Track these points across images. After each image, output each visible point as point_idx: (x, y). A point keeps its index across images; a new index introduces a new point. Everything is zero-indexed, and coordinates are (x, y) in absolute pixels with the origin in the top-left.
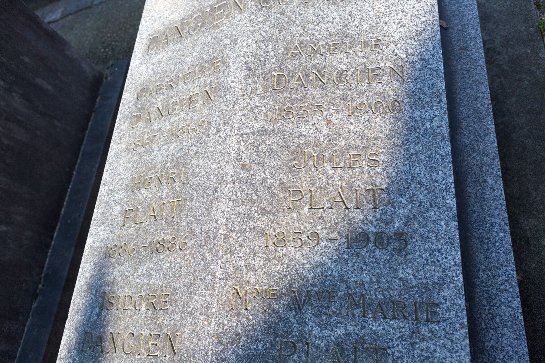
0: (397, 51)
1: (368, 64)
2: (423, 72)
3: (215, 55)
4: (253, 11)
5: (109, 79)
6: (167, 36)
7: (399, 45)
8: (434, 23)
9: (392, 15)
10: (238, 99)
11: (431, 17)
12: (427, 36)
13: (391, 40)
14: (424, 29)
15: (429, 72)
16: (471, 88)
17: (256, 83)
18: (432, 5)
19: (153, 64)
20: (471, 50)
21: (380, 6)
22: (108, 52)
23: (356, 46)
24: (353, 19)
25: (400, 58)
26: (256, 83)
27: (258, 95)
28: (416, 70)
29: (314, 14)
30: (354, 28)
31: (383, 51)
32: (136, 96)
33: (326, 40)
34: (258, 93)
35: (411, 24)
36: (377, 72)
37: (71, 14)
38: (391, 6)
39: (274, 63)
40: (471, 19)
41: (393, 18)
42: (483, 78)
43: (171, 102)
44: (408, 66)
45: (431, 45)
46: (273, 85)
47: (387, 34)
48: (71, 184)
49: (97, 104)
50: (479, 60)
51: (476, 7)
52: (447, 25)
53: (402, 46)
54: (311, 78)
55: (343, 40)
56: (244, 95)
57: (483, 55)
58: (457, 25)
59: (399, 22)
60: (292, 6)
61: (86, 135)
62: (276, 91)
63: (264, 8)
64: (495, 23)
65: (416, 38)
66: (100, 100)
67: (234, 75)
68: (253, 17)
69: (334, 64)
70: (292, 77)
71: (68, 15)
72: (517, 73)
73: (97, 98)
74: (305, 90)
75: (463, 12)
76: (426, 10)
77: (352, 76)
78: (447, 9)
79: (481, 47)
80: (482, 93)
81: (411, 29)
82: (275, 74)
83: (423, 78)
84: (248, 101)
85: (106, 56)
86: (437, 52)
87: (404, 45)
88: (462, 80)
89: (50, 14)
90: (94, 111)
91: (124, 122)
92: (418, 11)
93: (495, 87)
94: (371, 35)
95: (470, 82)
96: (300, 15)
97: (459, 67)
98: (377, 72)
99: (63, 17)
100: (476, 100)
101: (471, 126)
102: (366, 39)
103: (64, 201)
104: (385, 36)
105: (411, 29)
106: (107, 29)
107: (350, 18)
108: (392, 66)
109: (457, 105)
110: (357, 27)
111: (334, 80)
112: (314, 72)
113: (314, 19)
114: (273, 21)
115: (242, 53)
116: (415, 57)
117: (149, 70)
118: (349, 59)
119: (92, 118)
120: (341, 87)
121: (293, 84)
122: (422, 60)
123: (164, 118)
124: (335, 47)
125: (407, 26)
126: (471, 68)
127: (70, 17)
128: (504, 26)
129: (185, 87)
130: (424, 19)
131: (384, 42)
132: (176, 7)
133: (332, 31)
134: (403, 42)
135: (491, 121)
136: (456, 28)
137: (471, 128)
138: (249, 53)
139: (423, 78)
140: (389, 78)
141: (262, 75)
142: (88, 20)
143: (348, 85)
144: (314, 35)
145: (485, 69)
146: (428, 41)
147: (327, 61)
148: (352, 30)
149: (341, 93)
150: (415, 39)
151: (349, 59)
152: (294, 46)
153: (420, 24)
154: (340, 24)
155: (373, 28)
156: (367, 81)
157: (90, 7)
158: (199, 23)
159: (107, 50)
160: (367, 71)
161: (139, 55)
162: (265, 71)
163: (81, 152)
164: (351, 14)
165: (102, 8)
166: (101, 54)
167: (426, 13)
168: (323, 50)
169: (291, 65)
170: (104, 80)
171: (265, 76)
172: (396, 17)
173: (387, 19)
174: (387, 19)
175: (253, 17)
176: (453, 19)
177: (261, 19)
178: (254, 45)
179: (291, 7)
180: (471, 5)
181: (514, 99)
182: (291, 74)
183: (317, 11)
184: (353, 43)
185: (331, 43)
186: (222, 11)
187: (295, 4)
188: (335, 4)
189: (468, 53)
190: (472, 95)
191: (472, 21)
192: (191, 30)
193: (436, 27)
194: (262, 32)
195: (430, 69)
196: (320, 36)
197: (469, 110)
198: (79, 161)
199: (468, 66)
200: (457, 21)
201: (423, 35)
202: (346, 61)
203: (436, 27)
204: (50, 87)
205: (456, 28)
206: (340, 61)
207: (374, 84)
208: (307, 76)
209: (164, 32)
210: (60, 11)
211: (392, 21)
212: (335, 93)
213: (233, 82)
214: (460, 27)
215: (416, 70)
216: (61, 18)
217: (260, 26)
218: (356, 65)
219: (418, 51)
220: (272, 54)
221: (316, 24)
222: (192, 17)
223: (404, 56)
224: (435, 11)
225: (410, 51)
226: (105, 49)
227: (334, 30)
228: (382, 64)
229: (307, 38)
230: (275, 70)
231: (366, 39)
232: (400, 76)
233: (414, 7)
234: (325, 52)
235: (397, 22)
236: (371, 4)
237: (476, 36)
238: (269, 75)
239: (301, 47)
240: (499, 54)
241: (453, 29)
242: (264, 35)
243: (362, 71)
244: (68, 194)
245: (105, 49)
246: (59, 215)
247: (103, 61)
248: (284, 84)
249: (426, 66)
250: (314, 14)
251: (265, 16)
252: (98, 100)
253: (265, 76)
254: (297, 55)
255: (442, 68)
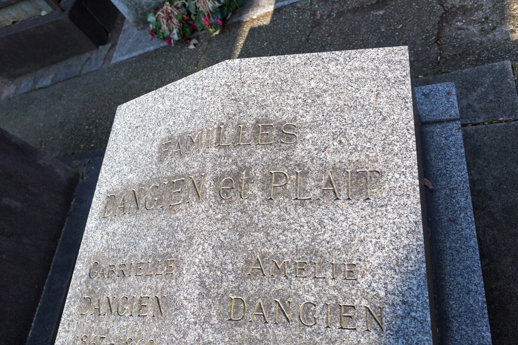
0: (374, 285)
1: (340, 300)
2: (405, 321)
3: (169, 250)
4: (211, 204)
5: (85, 178)
6: (124, 200)
7: (377, 277)
8: (419, 250)
9: (369, 231)
10: (188, 327)
11: (415, 240)
12: (410, 268)
13: (368, 266)
14: (407, 257)
15: (413, 323)
16: (463, 277)
17: (210, 307)
18: (416, 223)
19: (108, 234)
20: (461, 224)
21: (355, 215)
22: (92, 129)
23: (326, 271)
24: (323, 230)
25: (377, 295)
26: (210, 307)
27: (212, 325)
28: (397, 317)
29: (279, 217)
30: (324, 243)
31: (358, 283)
32: (88, 272)
33: (292, 257)
34: (212, 322)
35: (391, 247)
36: (351, 313)
37: (60, 82)
38: (367, 217)
39: (232, 281)
40: (460, 182)
41: (370, 235)
42: (476, 264)
43: (121, 296)
44: (387, 310)
45: (415, 282)
46: (230, 314)
47: (363, 258)
48: (41, 301)
49: (72, 207)
50: (471, 239)
51: (466, 167)
52: (433, 186)
53: (380, 278)
54: (273, 310)
55: (311, 258)
56: (195, 323)
57: (475, 232)
58: (444, 188)
59: (377, 242)
60: (255, 203)
61: (59, 244)
62: (233, 322)
63: (224, 202)
64: (485, 159)
65: (397, 268)
66: (75, 202)
67: (187, 290)
68: (211, 211)
69: (301, 293)
70: (252, 304)
71: (57, 82)
72: (512, 227)
73: (72, 201)
74: (266, 327)
75: (450, 171)
76: (408, 229)
77: (321, 314)
78: (433, 165)
79: (472, 222)
80: (475, 285)
81: (391, 255)
82: (233, 297)
83: (406, 331)
84: (200, 332)
85: (90, 134)
86: (421, 293)
87: (383, 277)
88: (452, 263)
89: (41, 80)
90: (69, 216)
91: (75, 302)
92: (399, 228)
93: (488, 241)
94: (344, 256)
95: (461, 267)
96: (264, 216)
97: (448, 245)
98: (351, 313)
99: (53, 84)
100: (468, 293)
101: (463, 329)
102: (338, 262)
103: (32, 322)
104: (360, 260)
105: (391, 255)
106: (93, 104)
107: (320, 228)
108: (368, 306)
109: (446, 296)
110: (328, 243)
111: (299, 317)
112: (277, 300)
113: (279, 223)
114: (233, 221)
115: (197, 260)
116: (396, 298)
117: (104, 241)
118: (318, 289)
119: (65, 224)
120: (308, 329)
121: (251, 315)
122: (404, 303)
123: (112, 317)
124: (301, 268)
125: (387, 249)
126: (461, 248)
127: (60, 85)
128: (496, 165)
129: (137, 282)
130: (406, 242)
131: (359, 269)
132: (135, 164)
133: (299, 243)
134: (381, 272)
135: (487, 326)
136: (443, 192)
137: (464, 333)
138: (204, 263)
139: (406, 331)
140: (365, 324)
141: (217, 296)
142: (75, 90)
143: (316, 326)
144: (278, 246)
145: (478, 253)
146: (411, 276)
147: (292, 287)
148: (322, 246)
149: (308, 337)
150: (395, 271)
151: (318, 289)
152: (255, 259)
153: (401, 249)
154: (308, 236)
155: (347, 245)
156: (338, 325)
157: (79, 76)
158: (156, 197)
159: (91, 127)
160: (338, 310)
161: (96, 215)
162: (221, 291)
163: (52, 264)
164: (321, 222)
165: (90, 79)
166: (86, 132)
167: (408, 232)
168: (288, 271)
169: (252, 286)
170: (80, 180)
171: (222, 298)
172: (373, 234)
173: (363, 235)
174: (363, 235)
175: (211, 211)
176: (440, 179)
177: (219, 216)
178: (211, 252)
179: (253, 204)
180: (460, 164)
181: (509, 260)
182: (251, 300)
183: (282, 213)
184: (323, 265)
185: (297, 261)
186: (180, 190)
187: (258, 200)
188: (303, 206)
189: (458, 227)
190: (464, 286)
191: (461, 185)
192: (147, 203)
193: (420, 255)
194: (220, 235)
195: (415, 318)
196: (285, 250)
197: (461, 307)
198: (50, 273)
199: (458, 245)
200: (444, 183)
201: (405, 265)
202: (315, 290)
203: (420, 255)
204: (18, 204)
205: (443, 192)
206: (306, 289)
207: (347, 331)
208: (269, 306)
209: (122, 194)
210: (51, 77)
211: (369, 240)
212: (301, 337)
213: (185, 299)
214: (448, 191)
215: (397, 317)
216: (51, 85)
217: (219, 225)
218: (326, 299)
219: (399, 289)
220: (230, 267)
221: (280, 231)
222: (150, 186)
223: (382, 294)
224: (420, 232)
225: (390, 287)
226: (89, 126)
227: (302, 243)
228: (357, 302)
229: (270, 250)
230: (232, 292)
231: (338, 262)
232: (379, 324)
233: (394, 223)
234: (290, 274)
235: (374, 241)
236: (344, 212)
237: (467, 206)
238: (225, 297)
239: (263, 262)
240: (490, 199)
241: (440, 192)
242: (222, 239)
243: (333, 309)
244: (37, 313)
245: (89, 126)
246: (26, 339)
247: (87, 140)
248: (243, 314)
249: (409, 313)
250: (279, 217)
251: (224, 212)
252: (72, 203)
253: (222, 298)
254: (258, 273)
255: (429, 319)
